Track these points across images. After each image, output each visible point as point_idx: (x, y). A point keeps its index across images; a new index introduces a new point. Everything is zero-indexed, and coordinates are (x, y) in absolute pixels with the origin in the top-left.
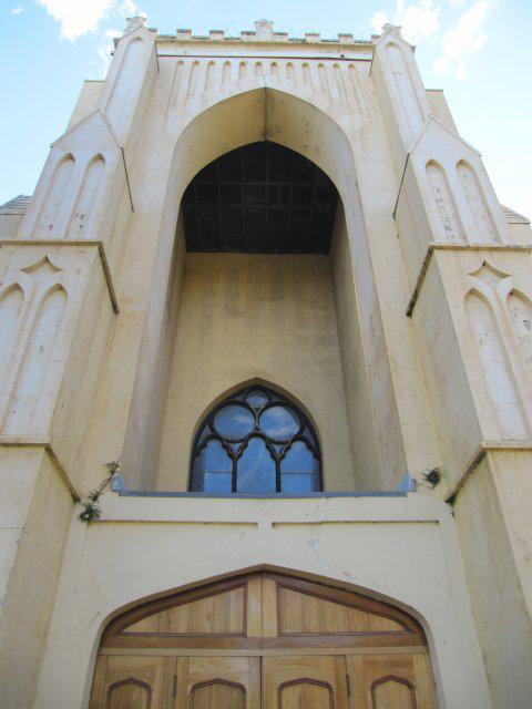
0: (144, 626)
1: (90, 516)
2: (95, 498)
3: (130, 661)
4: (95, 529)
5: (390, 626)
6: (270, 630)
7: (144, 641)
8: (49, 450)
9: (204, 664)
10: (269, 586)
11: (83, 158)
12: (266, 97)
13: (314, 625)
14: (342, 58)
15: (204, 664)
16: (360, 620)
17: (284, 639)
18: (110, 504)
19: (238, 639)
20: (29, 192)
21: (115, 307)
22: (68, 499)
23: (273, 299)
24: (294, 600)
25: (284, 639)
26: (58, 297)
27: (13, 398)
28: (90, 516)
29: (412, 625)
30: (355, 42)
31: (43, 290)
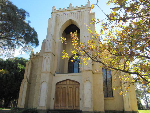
0: (59, 84)
1: (54, 76)
2: (55, 74)
3: (58, 86)
4: (55, 77)
5: (78, 83)
6: (68, 84)
7: (59, 85)
8: (50, 72)
9: (63, 86)
10: (68, 80)
11: (49, 40)
12: (71, 20)
13: (72, 83)
14: (81, 11)
15: (63, 86)
16: (75, 83)
17: (69, 85)
18: (56, 75)
19: (66, 85)
20: (45, 38)
21: (55, 56)
22: (52, 75)
23: (37, 110)
24: (70, 82)
25: (69, 85)
26: (49, 58)
27: (47, 68)
28: (54, 76)
29: (79, 83)
30: (84, 7)
31: (48, 57)
